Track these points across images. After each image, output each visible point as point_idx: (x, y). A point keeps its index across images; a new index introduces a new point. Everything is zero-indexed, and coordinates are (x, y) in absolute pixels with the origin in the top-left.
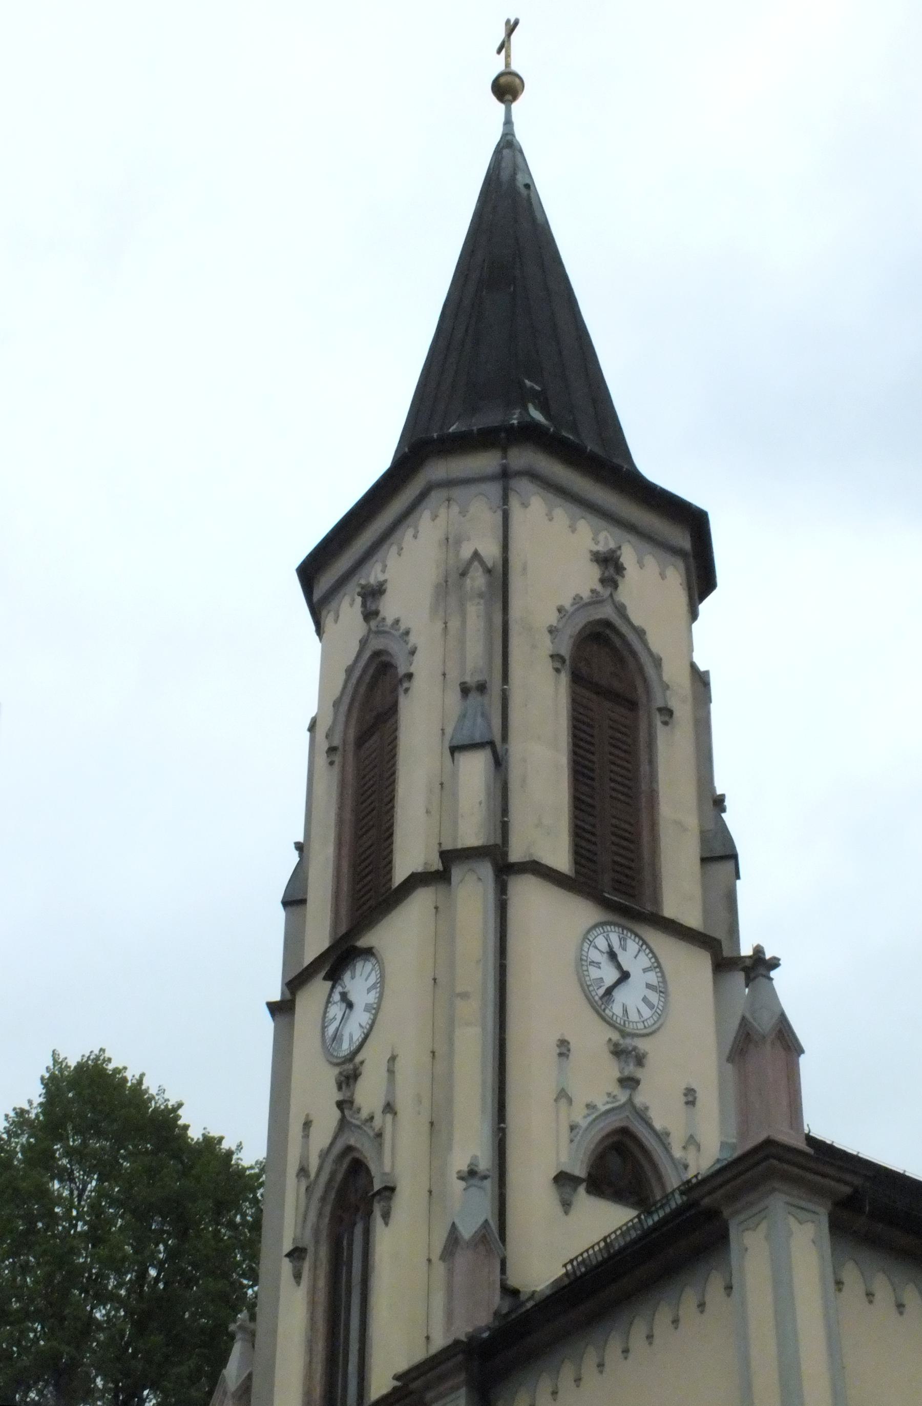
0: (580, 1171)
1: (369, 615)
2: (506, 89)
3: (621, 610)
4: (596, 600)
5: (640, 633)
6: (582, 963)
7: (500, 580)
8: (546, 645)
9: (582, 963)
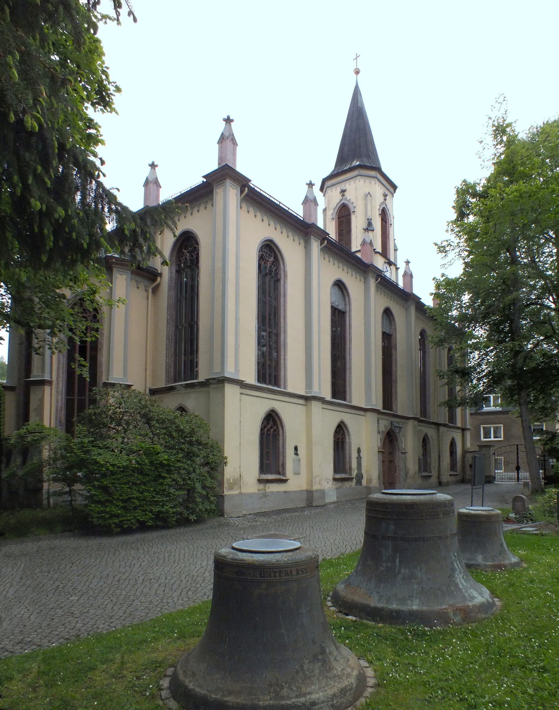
1: (343, 195)
2: (357, 72)
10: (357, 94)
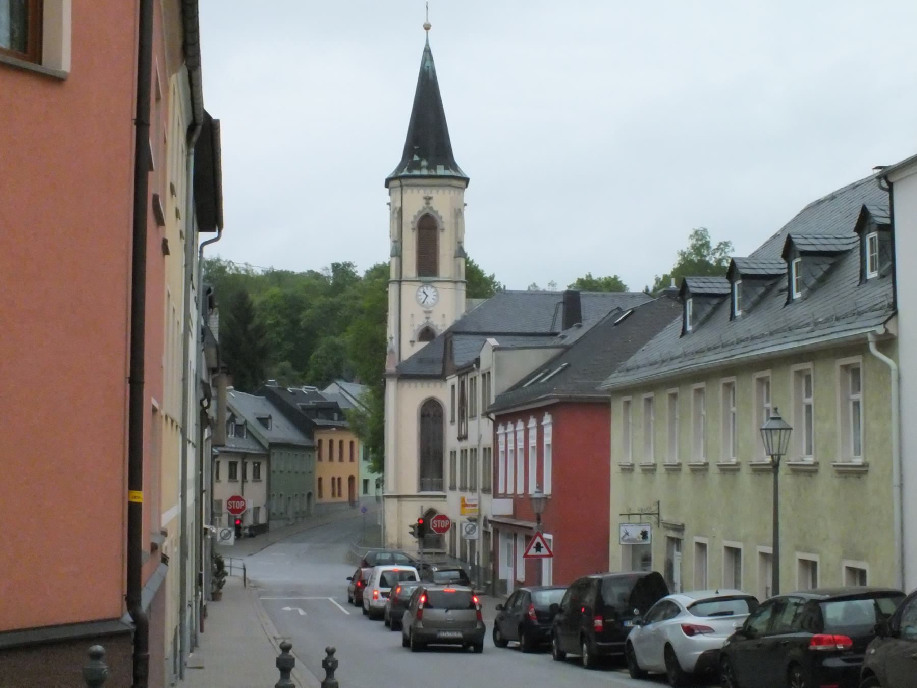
0: (416, 339)
2: (427, 27)
3: (431, 208)
4: (424, 209)
5: (436, 212)
6: (417, 295)
7: (401, 211)
8: (411, 226)
9: (417, 295)
10: (428, 52)
